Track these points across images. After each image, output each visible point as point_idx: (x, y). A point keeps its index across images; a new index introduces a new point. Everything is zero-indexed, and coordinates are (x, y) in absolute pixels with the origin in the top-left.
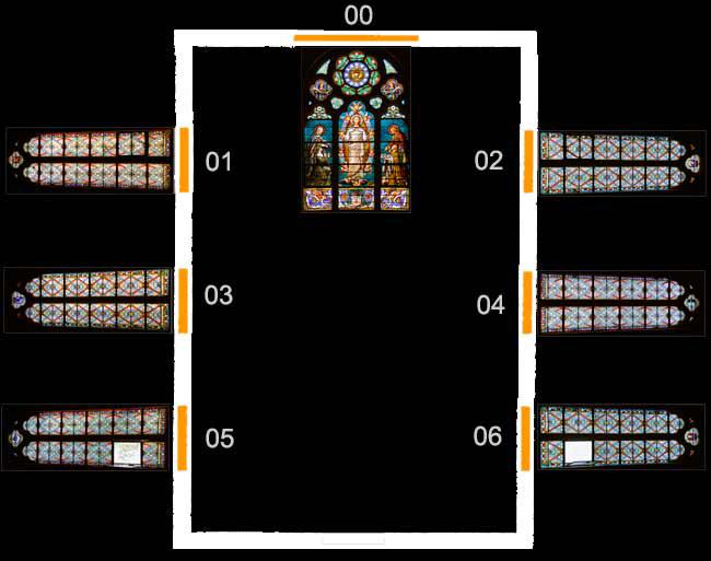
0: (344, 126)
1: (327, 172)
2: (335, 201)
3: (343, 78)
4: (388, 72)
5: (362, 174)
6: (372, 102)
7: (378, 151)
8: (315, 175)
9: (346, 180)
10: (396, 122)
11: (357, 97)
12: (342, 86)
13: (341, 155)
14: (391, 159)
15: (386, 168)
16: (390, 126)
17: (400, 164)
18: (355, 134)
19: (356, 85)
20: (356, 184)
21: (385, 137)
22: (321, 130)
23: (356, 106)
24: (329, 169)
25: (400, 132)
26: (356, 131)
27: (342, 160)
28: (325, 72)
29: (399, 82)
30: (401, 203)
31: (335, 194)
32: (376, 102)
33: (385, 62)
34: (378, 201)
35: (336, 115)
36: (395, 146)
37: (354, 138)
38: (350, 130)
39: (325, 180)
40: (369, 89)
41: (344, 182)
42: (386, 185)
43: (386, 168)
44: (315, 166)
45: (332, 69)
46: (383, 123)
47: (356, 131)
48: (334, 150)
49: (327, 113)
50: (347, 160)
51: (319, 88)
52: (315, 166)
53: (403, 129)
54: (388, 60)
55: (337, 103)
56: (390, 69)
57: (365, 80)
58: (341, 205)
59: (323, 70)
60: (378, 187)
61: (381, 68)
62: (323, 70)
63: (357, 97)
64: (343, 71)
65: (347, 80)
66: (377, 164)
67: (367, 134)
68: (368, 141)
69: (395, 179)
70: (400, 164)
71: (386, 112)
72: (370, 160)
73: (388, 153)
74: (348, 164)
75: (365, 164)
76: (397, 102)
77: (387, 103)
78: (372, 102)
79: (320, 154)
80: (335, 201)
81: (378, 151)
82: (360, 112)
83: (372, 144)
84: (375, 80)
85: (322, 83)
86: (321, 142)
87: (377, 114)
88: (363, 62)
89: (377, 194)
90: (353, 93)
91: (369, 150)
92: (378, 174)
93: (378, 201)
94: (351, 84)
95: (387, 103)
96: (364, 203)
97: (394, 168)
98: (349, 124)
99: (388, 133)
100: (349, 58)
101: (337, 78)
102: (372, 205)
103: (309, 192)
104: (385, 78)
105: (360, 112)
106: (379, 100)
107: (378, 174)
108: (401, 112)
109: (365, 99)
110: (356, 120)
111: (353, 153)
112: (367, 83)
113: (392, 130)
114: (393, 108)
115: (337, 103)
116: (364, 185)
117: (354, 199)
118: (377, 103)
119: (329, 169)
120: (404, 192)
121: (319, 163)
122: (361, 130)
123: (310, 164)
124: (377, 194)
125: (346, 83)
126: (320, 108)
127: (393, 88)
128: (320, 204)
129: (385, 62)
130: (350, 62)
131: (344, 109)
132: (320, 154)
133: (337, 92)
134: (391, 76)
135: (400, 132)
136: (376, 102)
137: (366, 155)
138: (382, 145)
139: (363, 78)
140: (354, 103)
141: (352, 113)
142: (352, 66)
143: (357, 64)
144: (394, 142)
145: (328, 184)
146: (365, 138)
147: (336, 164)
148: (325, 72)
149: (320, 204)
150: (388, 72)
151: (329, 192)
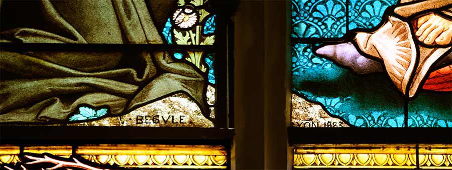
9: (391, 48)
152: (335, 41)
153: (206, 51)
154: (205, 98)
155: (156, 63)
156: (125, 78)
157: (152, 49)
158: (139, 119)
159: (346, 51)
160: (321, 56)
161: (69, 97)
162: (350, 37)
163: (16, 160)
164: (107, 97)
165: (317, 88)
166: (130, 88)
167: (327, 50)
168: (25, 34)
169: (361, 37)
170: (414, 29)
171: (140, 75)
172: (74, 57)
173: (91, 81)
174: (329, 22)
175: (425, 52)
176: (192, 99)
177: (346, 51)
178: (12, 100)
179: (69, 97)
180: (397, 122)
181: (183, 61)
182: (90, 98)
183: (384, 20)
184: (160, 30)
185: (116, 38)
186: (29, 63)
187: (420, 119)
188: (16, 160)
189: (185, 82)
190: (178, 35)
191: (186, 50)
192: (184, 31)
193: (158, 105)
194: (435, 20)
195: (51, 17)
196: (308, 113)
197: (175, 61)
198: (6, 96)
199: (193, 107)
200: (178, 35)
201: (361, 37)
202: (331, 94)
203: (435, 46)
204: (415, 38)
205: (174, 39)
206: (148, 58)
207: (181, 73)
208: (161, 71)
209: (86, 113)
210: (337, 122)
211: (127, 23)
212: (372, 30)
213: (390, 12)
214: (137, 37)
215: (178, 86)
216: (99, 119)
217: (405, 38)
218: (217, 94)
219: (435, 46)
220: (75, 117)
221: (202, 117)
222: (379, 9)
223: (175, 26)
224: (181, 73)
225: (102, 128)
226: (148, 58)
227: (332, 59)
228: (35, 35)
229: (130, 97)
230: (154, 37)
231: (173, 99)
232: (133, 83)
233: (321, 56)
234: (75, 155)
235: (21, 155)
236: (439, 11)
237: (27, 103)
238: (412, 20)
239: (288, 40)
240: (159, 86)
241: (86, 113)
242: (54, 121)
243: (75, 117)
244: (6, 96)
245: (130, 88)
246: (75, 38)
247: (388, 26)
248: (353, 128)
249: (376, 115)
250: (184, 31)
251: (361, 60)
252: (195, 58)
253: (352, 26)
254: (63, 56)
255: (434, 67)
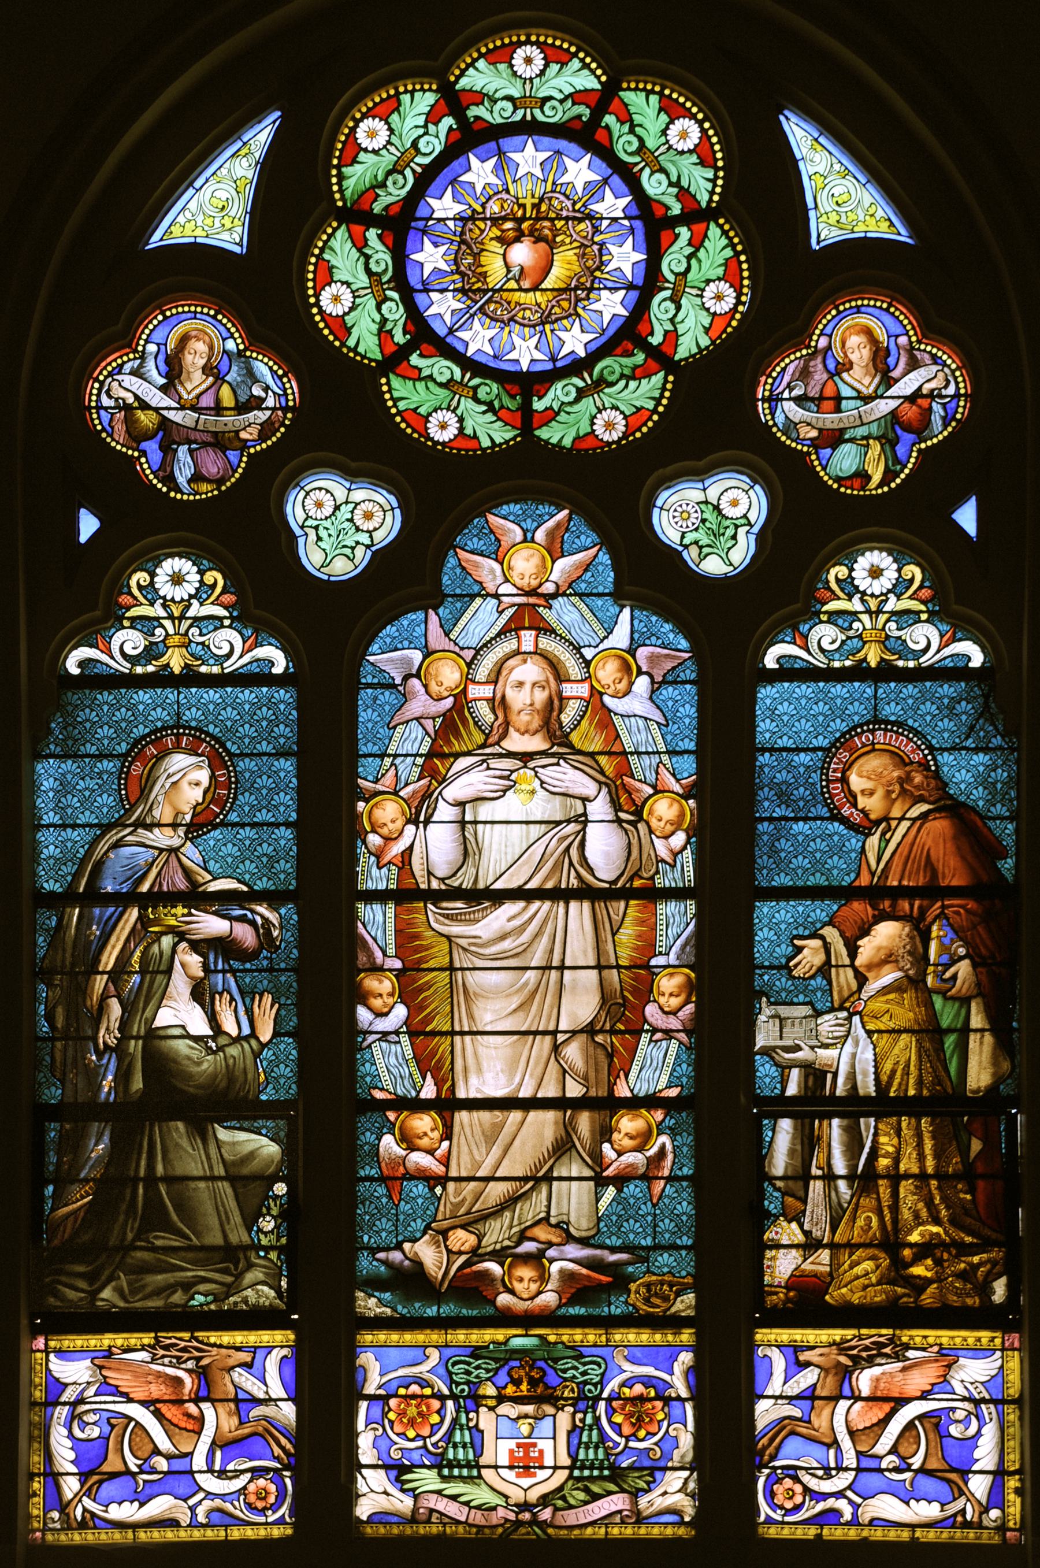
0: (412, 740)
1: (246, 1181)
2: (321, 1457)
3: (403, 283)
4: (824, 230)
5: (574, 1200)
6: (676, 514)
7: (727, 983)
8: (137, 1208)
9: (428, 1253)
10: (896, 701)
11: (529, 471)
12: (395, 360)
13: (380, 1013)
14: (854, 1058)
15: (808, 1143)
16: (844, 745)
17: (941, 1103)
18: (509, 819)
19: (525, 352)
20: (526, 1290)
21: (803, 847)
22: (186, 779)
23: (520, 553)
24: (263, 1146)
25: (949, 806)
26: (523, 782)
27: (389, 1066)
28: (230, 235)
29: (931, 328)
30: (953, 1473)
31: (327, 1389)
32: (714, 519)
33: (799, 133)
34: (730, 1454)
35: (328, 633)
36: (886, 934)
37: (508, 851)
38: (468, 780)
39: (232, 1258)
40: (646, 392)
41: (411, 1280)
42: (808, 1304)
43: (808, 1143)
44: (132, 1120)
45: (295, 202)
46: (781, 714)
47: (523, 782)
48: (318, 978)
49: (251, 616)
50: (444, 1076)
51: (173, 380)
52: (132, 1120)
53: (965, 773)
54: (809, 114)
55: (338, 523)
56: (842, 200)
57: (611, 306)
58: (375, 1495)
59: (213, 208)
60: (729, 1314)
61: (761, 198)
62: (213, 208)
63: (529, 471)
64: (402, 225)
65: (441, 307)
66: (722, 1102)
67: (629, 811)
68: (639, 890)
69: (890, 1242)
70: (941, 1103)
71: (112, 616)
72: (656, 1067)
73: (820, 995)
74: (447, 1106)
75: (607, 1106)
76: (905, 518)
77: (810, 526)
78: (676, 514)
79: (179, 1013)
80: (321, 1457)
81: (727, 983)
82: (565, 614)
83: (676, 921)
84: (704, 300)
85: (202, 334)
86: (196, 897)
87: (724, 632)
88: (585, 135)
89: (724, 1389)
90: (493, 432)
91: (642, 976)
92: (730, 1201)
93: (730, 1454)
94: (478, 339)
95: (810, 526)
96: (601, 1471)
97: (883, 1137)
98: (453, 722)
99: (835, 808)
100: (453, 101)
101: (347, 291)
102: (673, 1493)
103: (74, 1372)
104: (794, 281)
105: (565, 614)
106: (742, 499)
107: (730, 1201)
108: (949, 608)
109: (607, 490)
110: (525, 684)
111: (494, 1000)
112: (629, 333)
113: (867, 781)
114: (874, 570)
115: (338, 523)
116: (594, 1296)
117: (500, 1431)
118: (718, 524)
119: (263, 1146)
120: (974, 1372)
121: (180, 1096)
122: (571, 778)
123: (85, 1112)
124: (724, 1389)
125: (423, 335)
126: (177, 577)
127: (872, 382)
128: (180, 1477)
129: (799, 133)
130: (471, 137)
131: (409, 578)
132: (179, 1013)
133: (341, 415)
134: (858, 265)
135: (949, 806)
136: (714, 519)
137: (621, 1018)
138: (772, 923)
139: (579, 291)
140: (506, 524)
141: (481, 620)
142: (480, 172)
143: (529, 157)
144: (880, 898)
145: (259, 1292)
146: (604, 850)
147: (328, 1107)
148: (230, 235)
149: (180, 1477)
150: (824, 230)
151: (266, 1373)
152: (388, 1249)
153: (280, 1249)
154: (280, 1286)
155: (247, 1259)
156: (225, 1271)
157: (245, 1248)
158: (236, 1303)
159: (396, 1256)
160: (378, 1260)
161: (188, 1287)
162: (399, 1247)
163: (153, 1341)
164: (214, 1286)
165: (374, 1284)
166: (229, 1279)
167: (381, 1255)
168: (157, 1237)
169: (407, 1246)
170: (446, 1239)
171: (236, 1269)
172: (190, 1255)
173: (202, 1273)
174: (384, 1235)
175: (454, 1257)
176: (271, 1287)
177: (396, 1256)
178: (149, 1289)
179: (188, 1287)
180: (431, 1311)
181: (265, 1258)
182: (202, 1288)
183: (424, 1233)
184: (250, 1232)
185: (219, 1241)
186: (159, 1260)
187: (448, 1310)
188: (153, 1341)
189: (265, 1274)
190: (262, 1237)
191: (267, 1249)
192: (266, 1234)
193: (249, 1292)
194: (460, 1233)
195: (175, 1224)
196: (369, 1305)
197: (260, 1257)
198: (144, 1287)
199: (272, 1293)
200: (262, 1237)
201: (407, 1246)
202: (384, 1290)
203: (460, 1253)
204: (446, 1247)
205: (259, 1240)
206: (241, 1256)
207: (264, 1267)
208: (250, 1266)
209: (200, 1299)
210: (388, 1311)
211: (227, 1227)
212: (415, 1241)
213: (428, 1227)
214: (234, 1239)
215: (261, 1276)
216: (208, 1304)
217: (439, 1246)
218: (288, 1283)
219: (460, 1253)
220: (192, 1303)
221: (278, 1301)
222: (420, 1224)
223: (260, 1230)
224: (264, 1267)
225: (211, 1311)
226: (241, 1256)
227: (385, 1262)
228: (163, 1238)
229: (229, 1286)
230: (245, 1238)
231: (259, 1287)
232: (231, 1275)
233: (378, 1260)
234: (193, 1337)
235: (156, 1338)
236: (463, 1227)
237: (158, 1292)
238: (444, 1233)
239: (353, 1247)
240: (250, 1277)
241: (200, 1299)
242: (177, 1306)
243: (192, 1303)
244: (144, 1287)
245: (229, 1279)
246: (189, 1239)
247: (427, 1237)
248: (403, 1316)
249: (417, 1305)
250: (266, 1234)
251: (407, 1263)
252: (273, 1255)
253: (400, 1238)
254: (183, 1254)
255: (460, 1269)
